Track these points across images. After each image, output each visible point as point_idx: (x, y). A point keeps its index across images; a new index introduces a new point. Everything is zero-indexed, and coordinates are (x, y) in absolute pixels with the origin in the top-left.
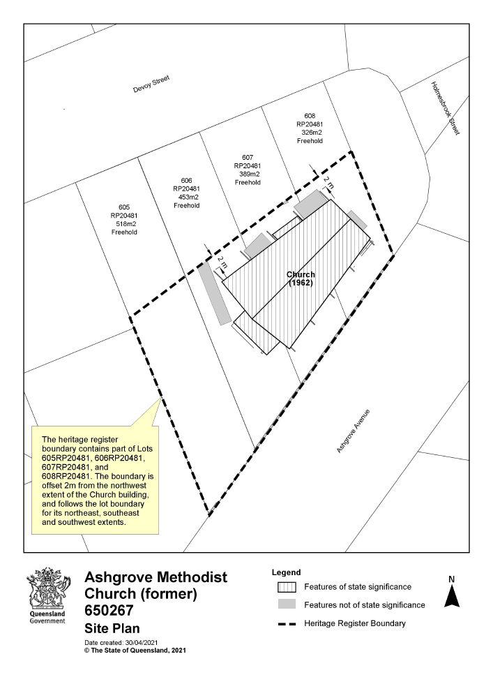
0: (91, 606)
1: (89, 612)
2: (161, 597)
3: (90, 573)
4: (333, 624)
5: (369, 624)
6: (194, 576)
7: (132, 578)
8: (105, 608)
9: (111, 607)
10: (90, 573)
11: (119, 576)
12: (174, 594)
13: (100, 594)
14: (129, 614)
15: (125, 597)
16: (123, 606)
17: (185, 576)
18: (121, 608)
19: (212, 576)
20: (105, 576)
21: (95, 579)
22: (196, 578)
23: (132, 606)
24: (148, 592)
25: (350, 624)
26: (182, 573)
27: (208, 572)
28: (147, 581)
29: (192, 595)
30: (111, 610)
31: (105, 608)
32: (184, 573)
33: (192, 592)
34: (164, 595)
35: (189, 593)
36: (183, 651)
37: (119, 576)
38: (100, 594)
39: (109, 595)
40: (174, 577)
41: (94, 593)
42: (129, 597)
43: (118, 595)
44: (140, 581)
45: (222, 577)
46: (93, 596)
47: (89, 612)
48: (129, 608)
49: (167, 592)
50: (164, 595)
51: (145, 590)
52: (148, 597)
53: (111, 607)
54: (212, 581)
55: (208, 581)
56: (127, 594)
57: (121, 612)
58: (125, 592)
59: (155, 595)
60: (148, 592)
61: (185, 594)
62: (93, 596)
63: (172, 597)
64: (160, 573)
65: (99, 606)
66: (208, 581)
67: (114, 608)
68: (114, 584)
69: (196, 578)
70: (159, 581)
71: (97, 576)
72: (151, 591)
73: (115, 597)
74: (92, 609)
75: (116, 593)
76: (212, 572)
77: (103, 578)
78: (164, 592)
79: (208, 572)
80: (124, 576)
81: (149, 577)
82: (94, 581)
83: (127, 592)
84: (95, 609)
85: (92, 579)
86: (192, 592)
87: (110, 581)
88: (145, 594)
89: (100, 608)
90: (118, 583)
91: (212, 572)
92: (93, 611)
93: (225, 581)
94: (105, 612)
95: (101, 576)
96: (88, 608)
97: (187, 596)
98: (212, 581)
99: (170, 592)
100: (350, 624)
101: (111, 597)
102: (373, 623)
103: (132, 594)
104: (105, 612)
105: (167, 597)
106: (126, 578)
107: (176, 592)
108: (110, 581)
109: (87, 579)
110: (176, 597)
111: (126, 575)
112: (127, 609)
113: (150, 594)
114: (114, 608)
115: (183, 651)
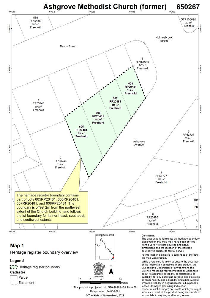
0: (179, 5)
1: (178, 8)
2: (150, 8)
3: (46, 5)
4: (30, 267)
5: (45, 267)
6: (95, 6)
7: (66, 7)
8: (186, 6)
9: (189, 5)
10: (46, 5)
11: (60, 6)
12: (156, 7)
13: (120, 7)
14: (197, 9)
15: (133, 8)
16: (195, 5)
17: (91, 6)
18: (194, 6)
19: (104, 6)
20: (53, 6)
21: (48, 7)
22: (96, 7)
23: (199, 5)
24: (143, 6)
25: (37, 267)
26: (90, 5)
27: (102, 4)
28: (73, 8)
29: (164, 7)
30: (189, 7)
31: (186, 6)
32: (91, 4)
33: (164, 6)
34: (151, 7)
35: (163, 6)
36: (123, 296)
37: (60, 6)
38: (120, 7)
39: (124, 7)
40: (86, 6)
41: (118, 6)
42: (134, 8)
43: (129, 7)
44: (70, 8)
45: (109, 7)
46: (117, 8)
47: (178, 8)
48: (198, 6)
49: (152, 6)
50: (151, 7)
51: (142, 5)
52: (143, 8)
53: (189, 5)
54: (104, 8)
55: (102, 8)
56: (133, 7)
57: (194, 8)
58: (132, 6)
59: (146, 7)
60: (143, 6)
61: (161, 7)
62: (117, 8)
63: (154, 8)
64: (79, 5)
65: (183, 5)
66: (102, 8)
67: (190, 6)
68: (58, 10)
69: (96, 7)
70: (79, 8)
71: (49, 6)
72: (145, 5)
73: (128, 8)
74: (180, 6)
75: (128, 6)
76: (104, 4)
77: (52, 7)
78: (151, 6)
79: (102, 4)
80: (62, 6)
81: (74, 6)
82: (48, 8)
83: (133, 6)
84: (181, 6)
85: (47, 7)
86: (164, 6)
87: (56, 8)
88: (142, 7)
89: (184, 6)
90: (59, 9)
91: (104, 4)
92: (181, 7)
93: (110, 8)
94: (186, 8)
95: (51, 6)
96: (178, 6)
97: (161, 8)
98: (104, 8)
99: (154, 6)
100: (37, 267)
101: (126, 8)
102: (94, 295)
103: (136, 7)
104: (186, 8)
105: (152, 8)
106: (63, 7)
107: (156, 6)
108: (56, 8)
109: (45, 7)
110: (157, 8)
111: (63, 6)
112: (196, 6)
113: (144, 7)
114: (190, 6)
115: (123, 296)
